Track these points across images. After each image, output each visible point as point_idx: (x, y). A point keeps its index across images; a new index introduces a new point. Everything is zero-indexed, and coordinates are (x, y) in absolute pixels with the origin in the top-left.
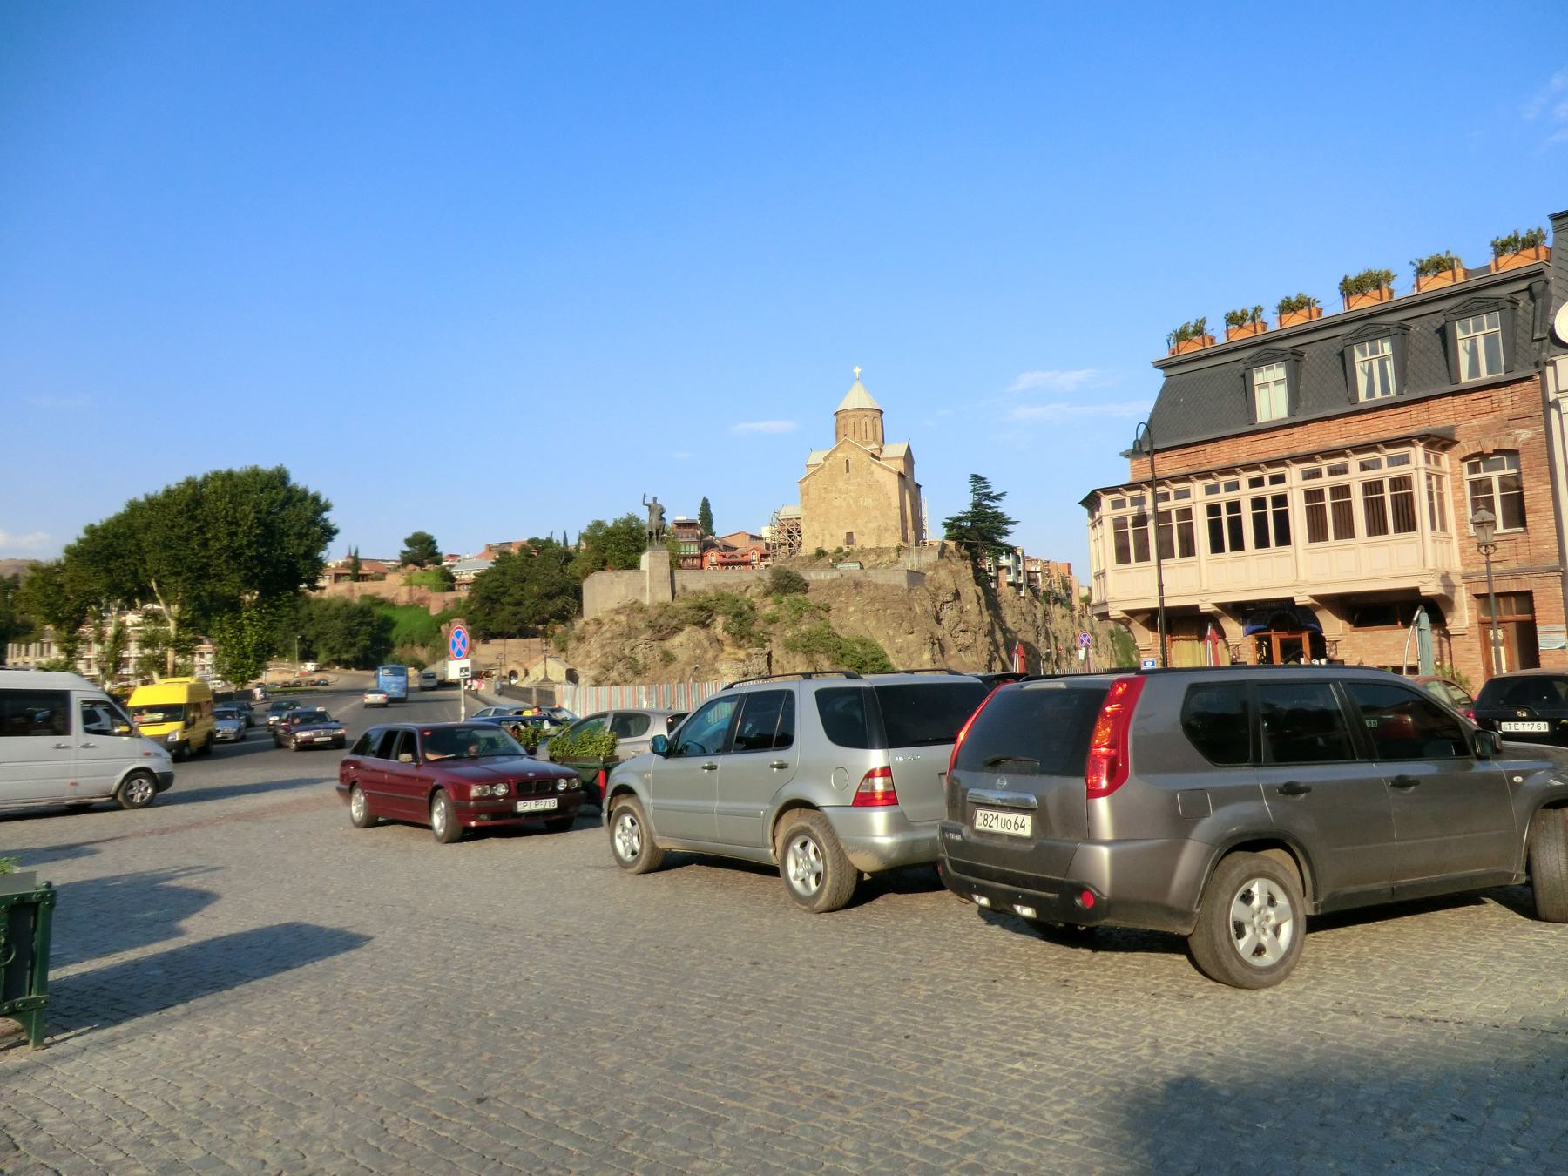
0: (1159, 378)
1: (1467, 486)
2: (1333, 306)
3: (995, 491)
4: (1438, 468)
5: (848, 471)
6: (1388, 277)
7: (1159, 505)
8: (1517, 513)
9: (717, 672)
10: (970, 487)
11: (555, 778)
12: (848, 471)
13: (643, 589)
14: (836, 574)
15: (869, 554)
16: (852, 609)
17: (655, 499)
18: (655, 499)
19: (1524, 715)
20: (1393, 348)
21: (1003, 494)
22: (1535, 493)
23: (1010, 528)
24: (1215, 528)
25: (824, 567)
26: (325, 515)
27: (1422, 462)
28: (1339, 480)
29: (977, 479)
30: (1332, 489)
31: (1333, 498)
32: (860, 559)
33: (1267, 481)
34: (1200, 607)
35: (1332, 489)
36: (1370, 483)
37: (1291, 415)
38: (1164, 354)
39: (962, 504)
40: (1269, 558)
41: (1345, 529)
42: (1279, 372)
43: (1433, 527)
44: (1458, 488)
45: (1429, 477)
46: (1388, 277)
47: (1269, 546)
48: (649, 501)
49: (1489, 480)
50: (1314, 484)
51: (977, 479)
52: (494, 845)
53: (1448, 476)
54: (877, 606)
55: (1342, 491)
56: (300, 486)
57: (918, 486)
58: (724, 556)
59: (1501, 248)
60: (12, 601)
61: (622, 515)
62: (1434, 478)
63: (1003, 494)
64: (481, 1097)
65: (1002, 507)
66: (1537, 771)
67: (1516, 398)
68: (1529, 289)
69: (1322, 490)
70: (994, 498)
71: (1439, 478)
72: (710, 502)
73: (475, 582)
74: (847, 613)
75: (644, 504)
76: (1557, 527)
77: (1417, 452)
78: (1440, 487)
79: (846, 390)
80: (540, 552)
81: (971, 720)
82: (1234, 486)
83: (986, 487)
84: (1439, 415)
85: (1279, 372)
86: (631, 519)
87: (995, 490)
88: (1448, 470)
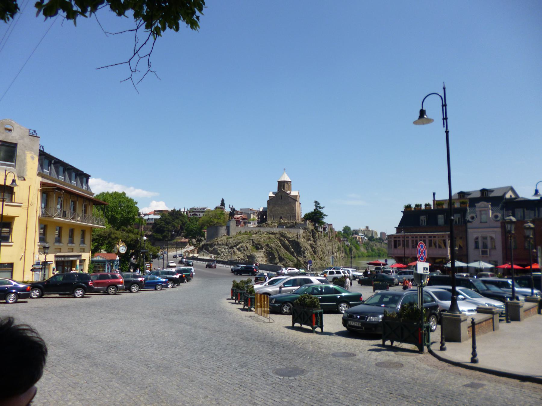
5: (282, 199)
10: (314, 204)
12: (282, 199)
17: (232, 206)
18: (232, 206)
21: (324, 207)
23: (325, 217)
26: (136, 205)
29: (316, 202)
51: (316, 202)
52: (115, 295)
56: (129, 197)
59: (444, 127)
60: (129, 246)
63: (324, 207)
64: (437, 396)
65: (323, 211)
66: (256, 227)
70: (320, 208)
72: (224, 200)
79: (282, 175)
83: (319, 205)
87: (321, 206)
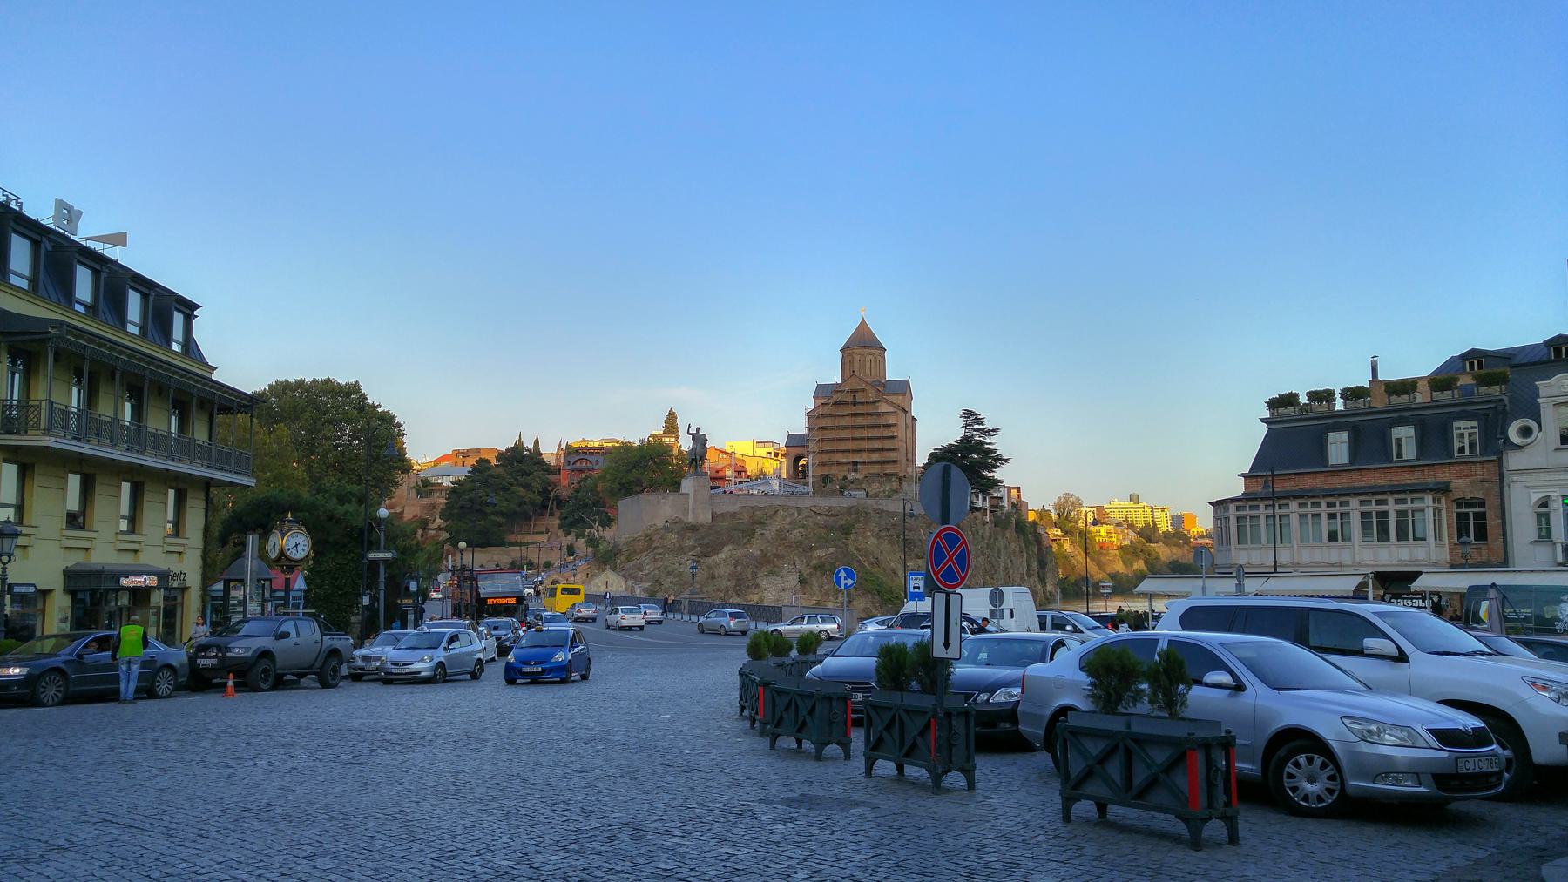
0: (1264, 429)
1: (1455, 515)
3: (989, 425)
4: (1439, 506)
7: (1272, 511)
8: (1482, 533)
9: (757, 586)
13: (687, 509)
17: (698, 429)
18: (698, 429)
21: (996, 430)
22: (1492, 522)
25: (833, 493)
27: (1431, 503)
30: (1377, 512)
32: (864, 486)
33: (1338, 504)
35: (1377, 512)
37: (1351, 463)
38: (1267, 415)
39: (953, 434)
42: (1345, 436)
43: (1436, 539)
44: (1449, 517)
45: (1434, 510)
48: (693, 431)
49: (1467, 514)
50: (1366, 508)
55: (1384, 514)
57: (914, 419)
62: (1437, 512)
63: (996, 430)
65: (997, 444)
68: (1496, 408)
71: (1440, 511)
73: (453, 491)
76: (1501, 493)
77: (1429, 498)
78: (1440, 516)
82: (1317, 505)
84: (1442, 476)
85: (1345, 436)
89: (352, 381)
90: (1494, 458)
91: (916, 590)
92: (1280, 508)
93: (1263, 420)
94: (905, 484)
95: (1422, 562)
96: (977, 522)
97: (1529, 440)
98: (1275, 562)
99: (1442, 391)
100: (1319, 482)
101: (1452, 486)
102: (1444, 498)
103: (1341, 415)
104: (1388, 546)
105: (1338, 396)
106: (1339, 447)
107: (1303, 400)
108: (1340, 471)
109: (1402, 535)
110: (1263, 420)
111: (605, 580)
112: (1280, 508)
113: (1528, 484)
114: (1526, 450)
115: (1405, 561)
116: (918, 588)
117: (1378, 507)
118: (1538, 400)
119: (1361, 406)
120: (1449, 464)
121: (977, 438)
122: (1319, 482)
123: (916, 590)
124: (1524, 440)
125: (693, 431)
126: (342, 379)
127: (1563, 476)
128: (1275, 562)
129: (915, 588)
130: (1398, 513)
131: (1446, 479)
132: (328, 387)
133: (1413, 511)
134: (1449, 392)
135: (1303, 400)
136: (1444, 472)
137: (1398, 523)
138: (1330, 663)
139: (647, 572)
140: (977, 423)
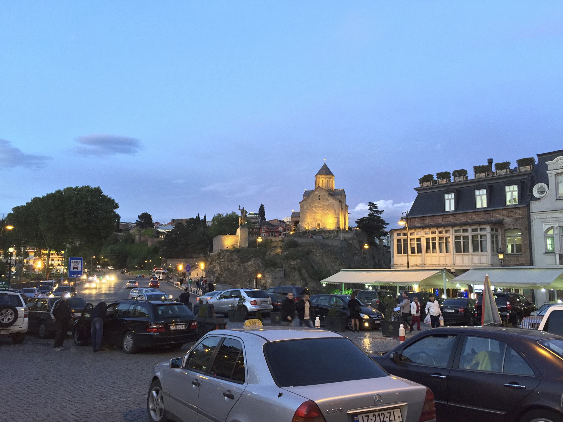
0: (416, 194)
2: (471, 176)
6: (508, 164)
11: (161, 296)
14: (312, 240)
15: (326, 232)
16: (318, 254)
17: (243, 208)
18: (243, 208)
19: (99, 267)
20: (487, 191)
24: (399, 246)
28: (465, 234)
31: (403, 242)
34: (451, 270)
35: (463, 237)
36: (404, 239)
40: (430, 256)
41: (466, 250)
46: (508, 164)
47: (402, 254)
50: (457, 234)
53: (500, 235)
54: (328, 254)
55: (465, 237)
58: (268, 229)
61: (230, 212)
67: (521, 213)
69: (401, 240)
71: (497, 236)
74: (316, 256)
75: (239, 210)
80: (196, 223)
81: (550, 334)
86: (234, 213)
88: (500, 233)
89: (97, 187)
90: (525, 206)
91: (75, 270)
92: (410, 235)
93: (416, 189)
94: (339, 233)
95: (485, 265)
96: (384, 251)
97: (543, 195)
98: (408, 263)
99: (501, 170)
100: (440, 221)
101: (505, 221)
102: (500, 229)
103: (453, 185)
104: (468, 255)
105: (451, 175)
106: (450, 203)
107: (435, 178)
108: (451, 214)
109: (475, 249)
110: (416, 189)
111: (197, 272)
112: (410, 235)
113: (542, 220)
114: (542, 200)
115: (477, 263)
116: (77, 268)
117: (464, 233)
118: (547, 172)
119: (462, 179)
120: (503, 209)
121: (375, 214)
122: (440, 221)
123: (75, 270)
124: (541, 196)
125: (241, 208)
126: (93, 186)
127: (558, 215)
128: (408, 263)
129: (74, 268)
130: (473, 237)
131: (501, 218)
132: (87, 189)
133: (481, 236)
134: (505, 170)
135: (435, 178)
136: (501, 214)
137: (473, 242)
138: (252, 334)
139: (217, 269)
140: (375, 208)
